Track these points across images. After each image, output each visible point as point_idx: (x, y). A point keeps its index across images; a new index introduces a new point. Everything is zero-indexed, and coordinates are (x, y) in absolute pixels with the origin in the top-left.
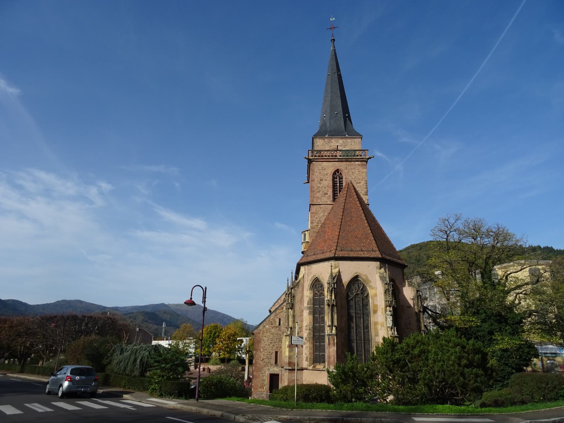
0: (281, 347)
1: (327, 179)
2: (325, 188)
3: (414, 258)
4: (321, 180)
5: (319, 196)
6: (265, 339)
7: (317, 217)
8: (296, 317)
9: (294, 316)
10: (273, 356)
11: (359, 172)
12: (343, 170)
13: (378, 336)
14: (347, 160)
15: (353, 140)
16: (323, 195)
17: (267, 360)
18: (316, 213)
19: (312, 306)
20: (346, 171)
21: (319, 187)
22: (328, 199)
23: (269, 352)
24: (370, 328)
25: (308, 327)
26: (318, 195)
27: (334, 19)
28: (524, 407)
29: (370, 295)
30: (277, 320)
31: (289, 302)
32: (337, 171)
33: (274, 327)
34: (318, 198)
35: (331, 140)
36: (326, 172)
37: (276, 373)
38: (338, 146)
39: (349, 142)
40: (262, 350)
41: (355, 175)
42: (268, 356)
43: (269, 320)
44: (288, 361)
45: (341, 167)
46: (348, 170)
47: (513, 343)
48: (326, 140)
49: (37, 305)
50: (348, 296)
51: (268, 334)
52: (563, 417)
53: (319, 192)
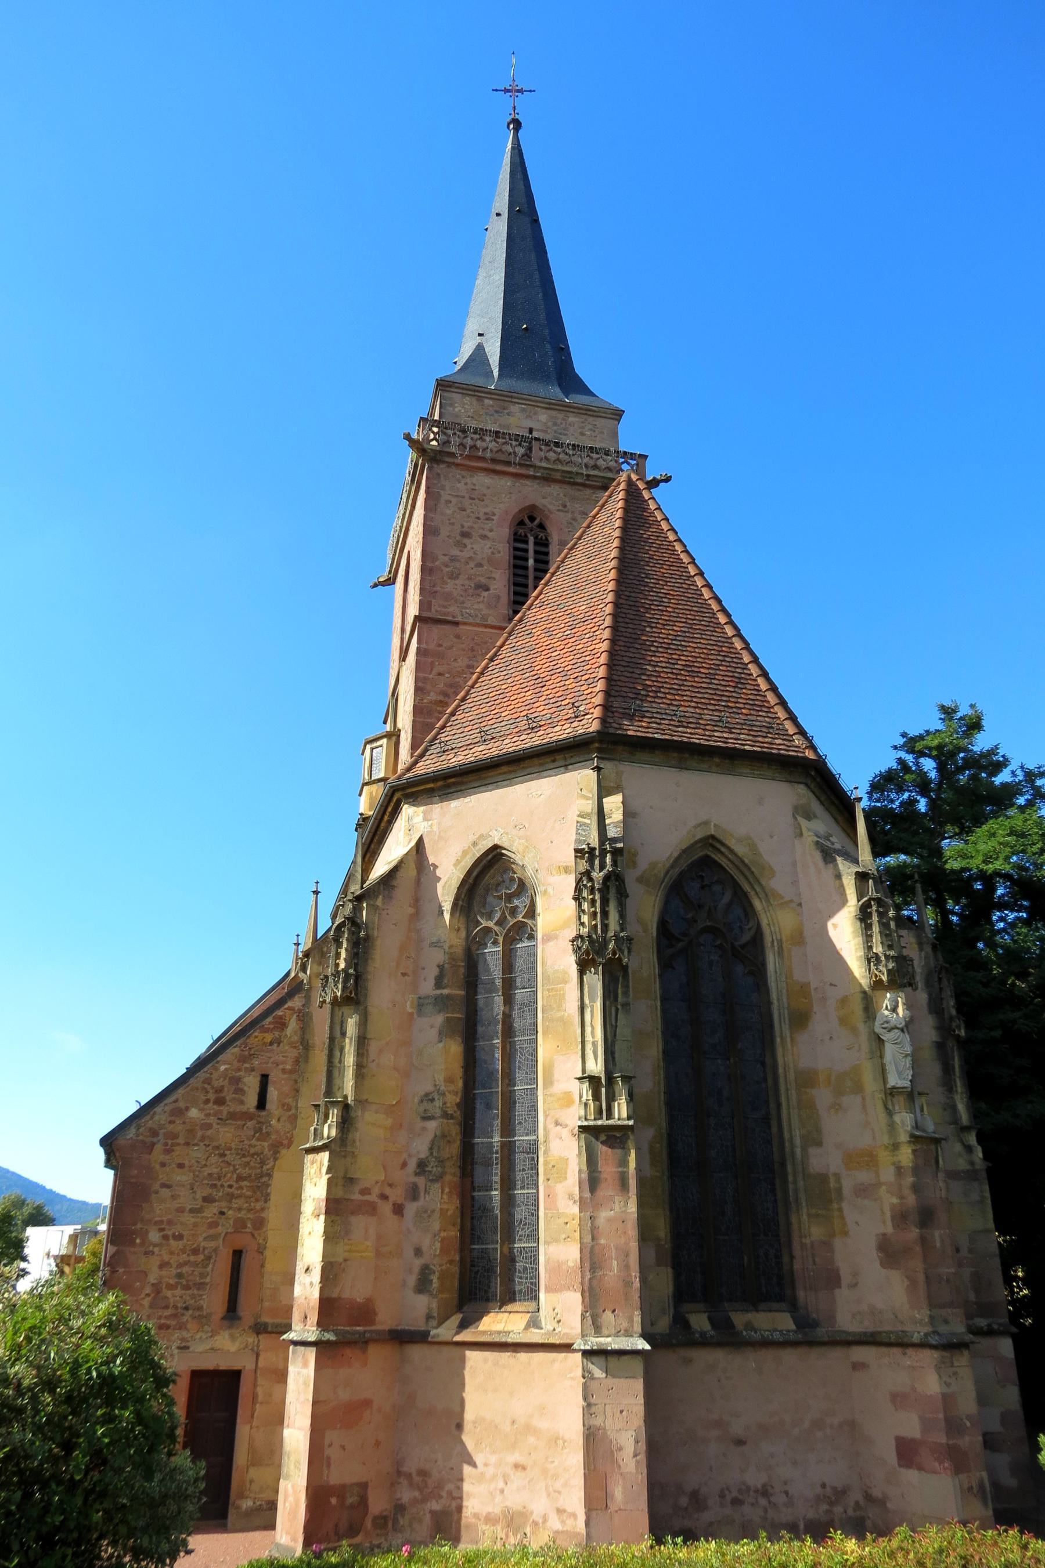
0: (260, 1223)
1: (490, 534)
2: (480, 565)
4: (465, 535)
5: (455, 593)
6: (182, 1177)
7: (441, 669)
8: (373, 1048)
9: (362, 1041)
10: (220, 1272)
12: (551, 512)
13: (819, 1144)
15: (591, 419)
16: (471, 591)
17: (179, 1292)
18: (441, 656)
19: (463, 993)
20: (564, 518)
21: (454, 559)
22: (489, 606)
23: (195, 1251)
24: (772, 1105)
25: (438, 1103)
26: (450, 586)
29: (768, 940)
30: (251, 1084)
31: (342, 966)
33: (233, 1116)
34: (448, 597)
35: (506, 404)
36: (487, 510)
37: (224, 1365)
39: (572, 424)
40: (154, 1236)
42: (185, 1270)
43: (207, 1081)
44: (316, 1294)
45: (544, 501)
46: (569, 515)
47: (59, 1283)
48: (486, 401)
51: (197, 1152)
53: (454, 576)
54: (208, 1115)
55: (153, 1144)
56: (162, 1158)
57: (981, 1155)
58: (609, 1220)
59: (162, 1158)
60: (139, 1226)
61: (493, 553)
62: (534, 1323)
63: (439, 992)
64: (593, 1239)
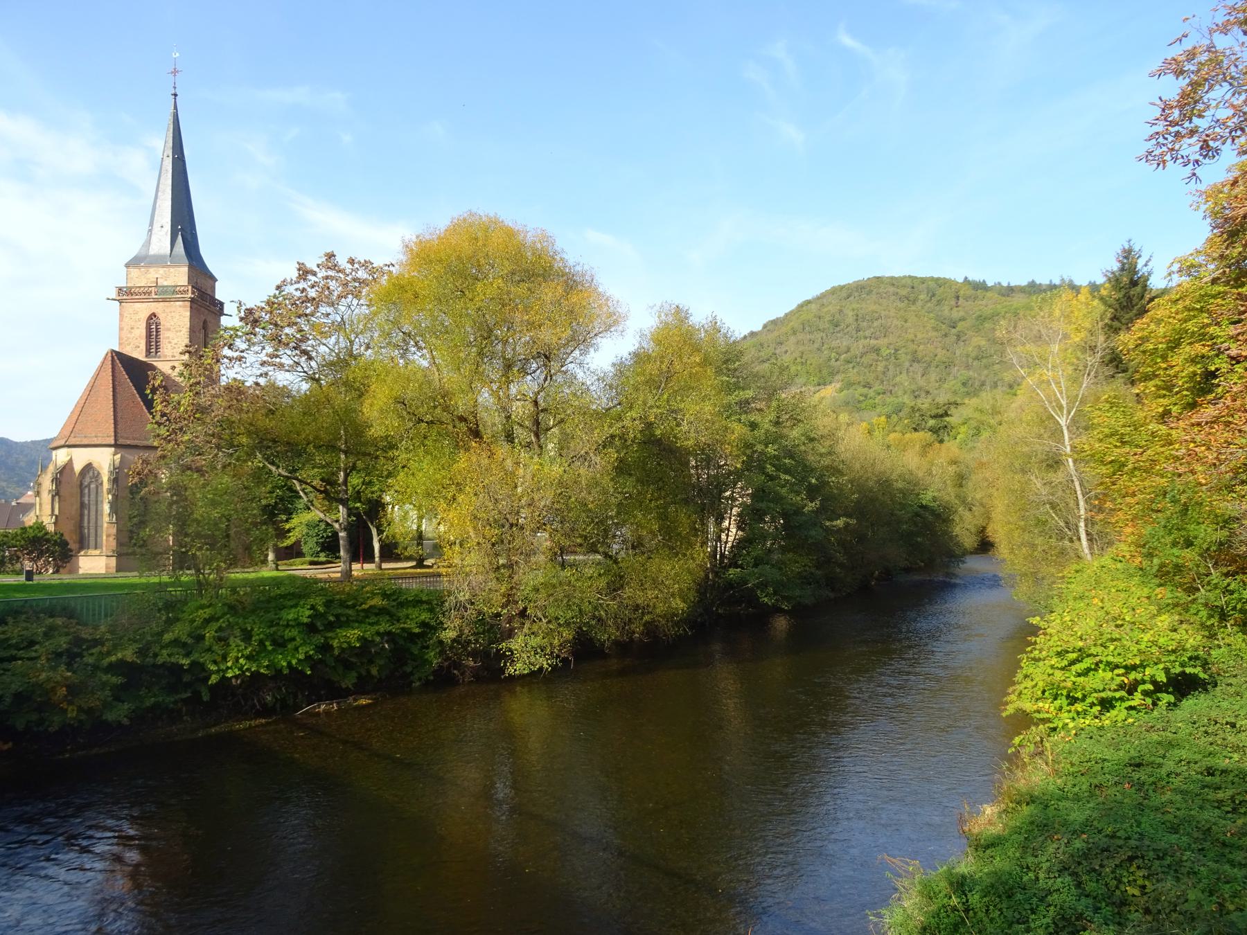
3: (828, 318)
4: (132, 328)
9: (40, 504)
14: (164, 300)
21: (128, 338)
27: (178, 55)
32: (154, 315)
41: (175, 320)
49: (33, 442)
50: (81, 484)
53: (129, 344)
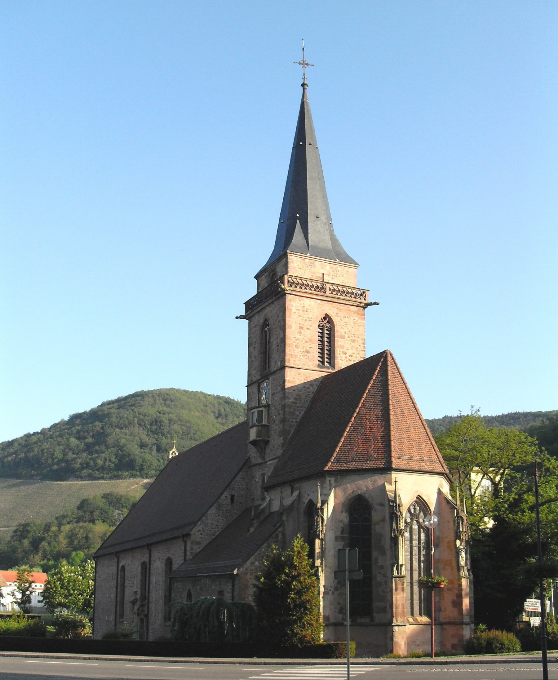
4: (301, 328)
11: (354, 323)
28: (406, 659)
38: (323, 274)
52: (0, 654)
54: (260, 564)
55: (247, 573)
56: (250, 577)
57: (472, 577)
58: (400, 598)
59: (250, 577)
60: (246, 595)
61: (311, 336)
62: (372, 620)
63: (342, 535)
64: (396, 602)
